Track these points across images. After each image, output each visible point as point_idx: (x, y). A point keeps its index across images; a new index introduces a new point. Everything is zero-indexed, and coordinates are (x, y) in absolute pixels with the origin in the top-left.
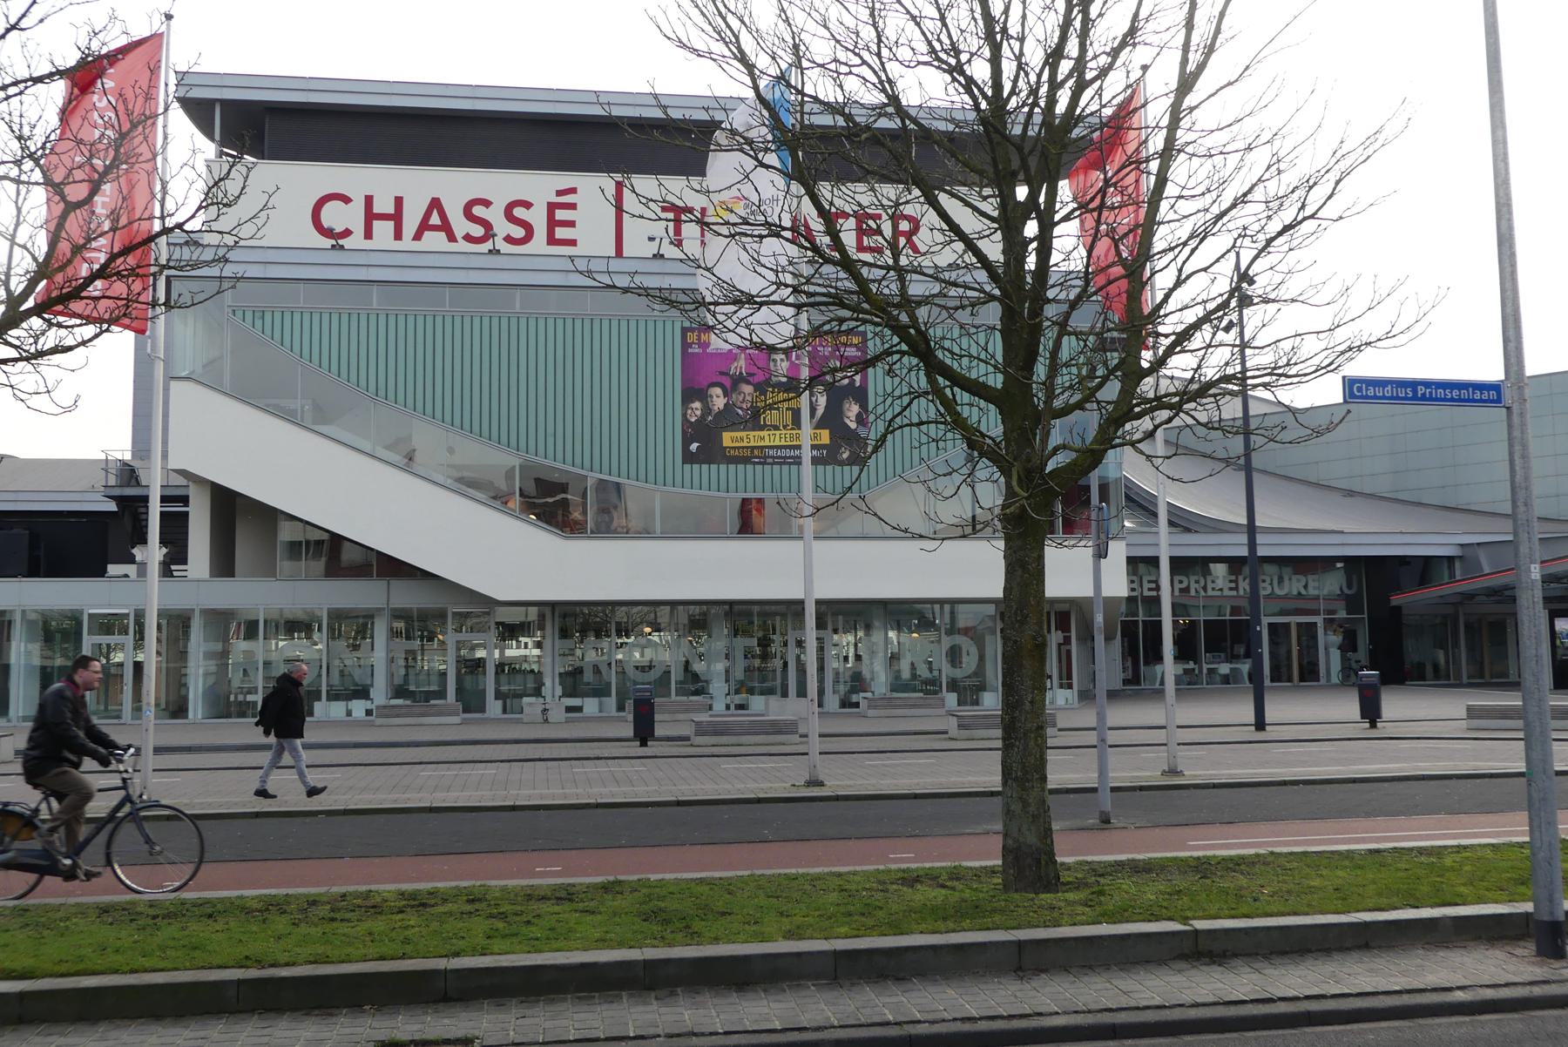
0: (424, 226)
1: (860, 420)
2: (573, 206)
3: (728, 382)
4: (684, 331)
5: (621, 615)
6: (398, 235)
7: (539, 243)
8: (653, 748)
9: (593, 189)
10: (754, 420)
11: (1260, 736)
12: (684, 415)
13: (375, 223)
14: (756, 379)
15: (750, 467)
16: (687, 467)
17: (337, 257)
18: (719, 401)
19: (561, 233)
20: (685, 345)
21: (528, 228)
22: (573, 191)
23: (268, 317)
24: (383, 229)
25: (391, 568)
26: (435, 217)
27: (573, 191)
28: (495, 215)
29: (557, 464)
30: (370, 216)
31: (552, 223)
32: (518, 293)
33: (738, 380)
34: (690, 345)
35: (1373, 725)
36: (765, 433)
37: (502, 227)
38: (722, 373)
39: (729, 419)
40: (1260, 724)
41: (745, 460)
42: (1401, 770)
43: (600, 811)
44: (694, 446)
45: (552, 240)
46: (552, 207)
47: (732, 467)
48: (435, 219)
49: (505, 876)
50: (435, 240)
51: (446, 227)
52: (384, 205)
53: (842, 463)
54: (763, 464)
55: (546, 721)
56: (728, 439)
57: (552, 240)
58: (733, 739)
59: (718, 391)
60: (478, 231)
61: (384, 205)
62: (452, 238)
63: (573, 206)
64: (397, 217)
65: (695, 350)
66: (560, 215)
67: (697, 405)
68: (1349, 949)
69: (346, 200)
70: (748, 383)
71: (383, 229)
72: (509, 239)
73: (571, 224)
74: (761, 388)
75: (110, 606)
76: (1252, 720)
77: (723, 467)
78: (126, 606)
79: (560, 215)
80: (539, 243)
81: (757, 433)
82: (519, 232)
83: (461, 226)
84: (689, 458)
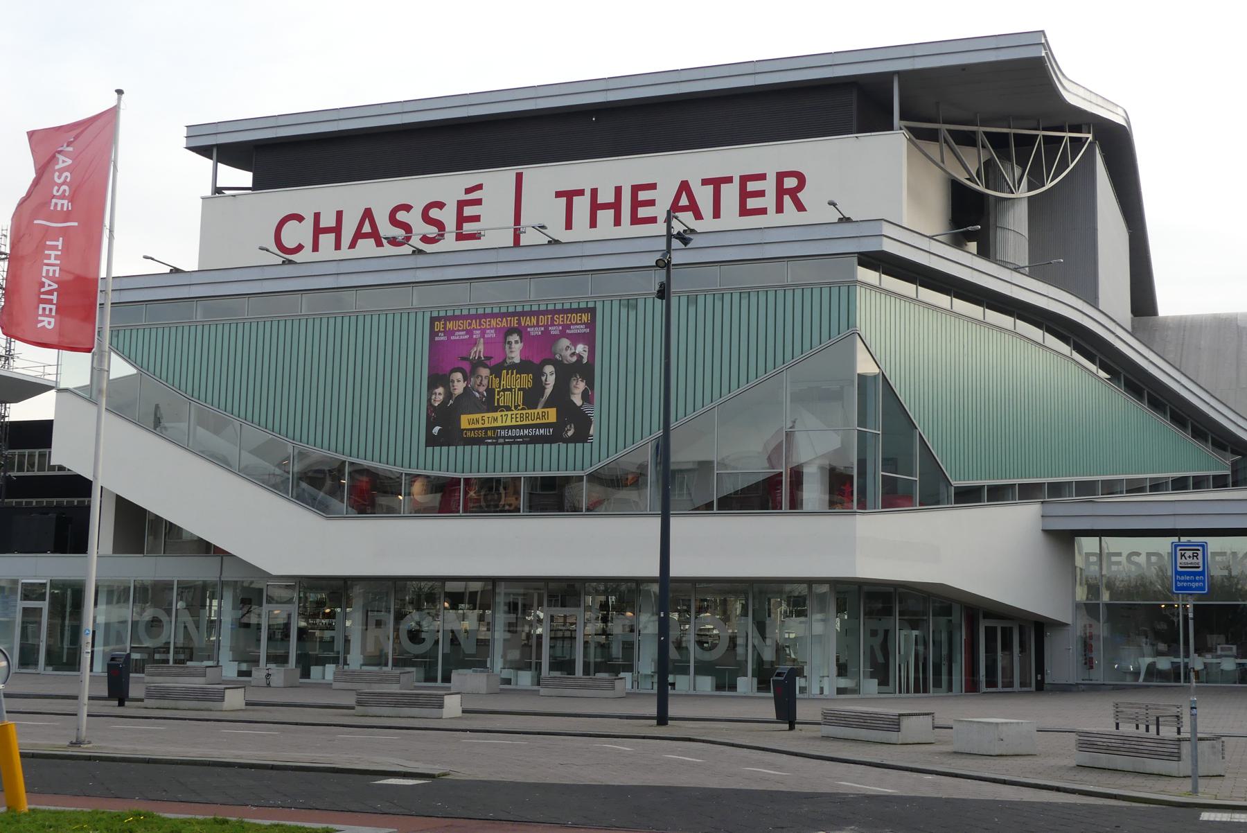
0: (675, 207)
1: (587, 397)
2: (478, 202)
3: (467, 368)
4: (433, 320)
5: (451, 587)
6: (338, 246)
7: (449, 242)
9: (496, 183)
10: (489, 404)
11: (120, 711)
12: (429, 400)
13: (321, 236)
14: (492, 363)
15: (483, 448)
16: (430, 449)
17: (288, 270)
18: (459, 387)
19: (468, 228)
20: (433, 334)
21: (440, 225)
22: (479, 187)
23: (727, 298)
24: (327, 240)
25: (205, 548)
26: (367, 228)
27: (479, 187)
28: (413, 218)
29: (320, 453)
30: (318, 231)
31: (461, 219)
32: (306, 297)
34: (437, 334)
35: (121, 704)
36: (498, 414)
38: (463, 359)
39: (467, 402)
42: (237, 756)
43: (274, 772)
44: (436, 430)
45: (460, 237)
46: (461, 204)
47: (468, 448)
48: (684, 201)
50: (366, 247)
51: (375, 235)
52: (328, 221)
54: (495, 444)
55: (269, 685)
56: (465, 421)
57: (460, 237)
59: (459, 376)
60: (399, 233)
61: (328, 221)
62: (379, 244)
63: (478, 202)
64: (337, 230)
66: (469, 211)
67: (440, 390)
69: (299, 218)
70: (485, 366)
71: (327, 240)
72: (425, 239)
73: (476, 219)
74: (497, 371)
75: (35, 577)
77: (460, 448)
78: (45, 577)
80: (449, 242)
81: (490, 415)
83: (386, 229)
84: (431, 441)
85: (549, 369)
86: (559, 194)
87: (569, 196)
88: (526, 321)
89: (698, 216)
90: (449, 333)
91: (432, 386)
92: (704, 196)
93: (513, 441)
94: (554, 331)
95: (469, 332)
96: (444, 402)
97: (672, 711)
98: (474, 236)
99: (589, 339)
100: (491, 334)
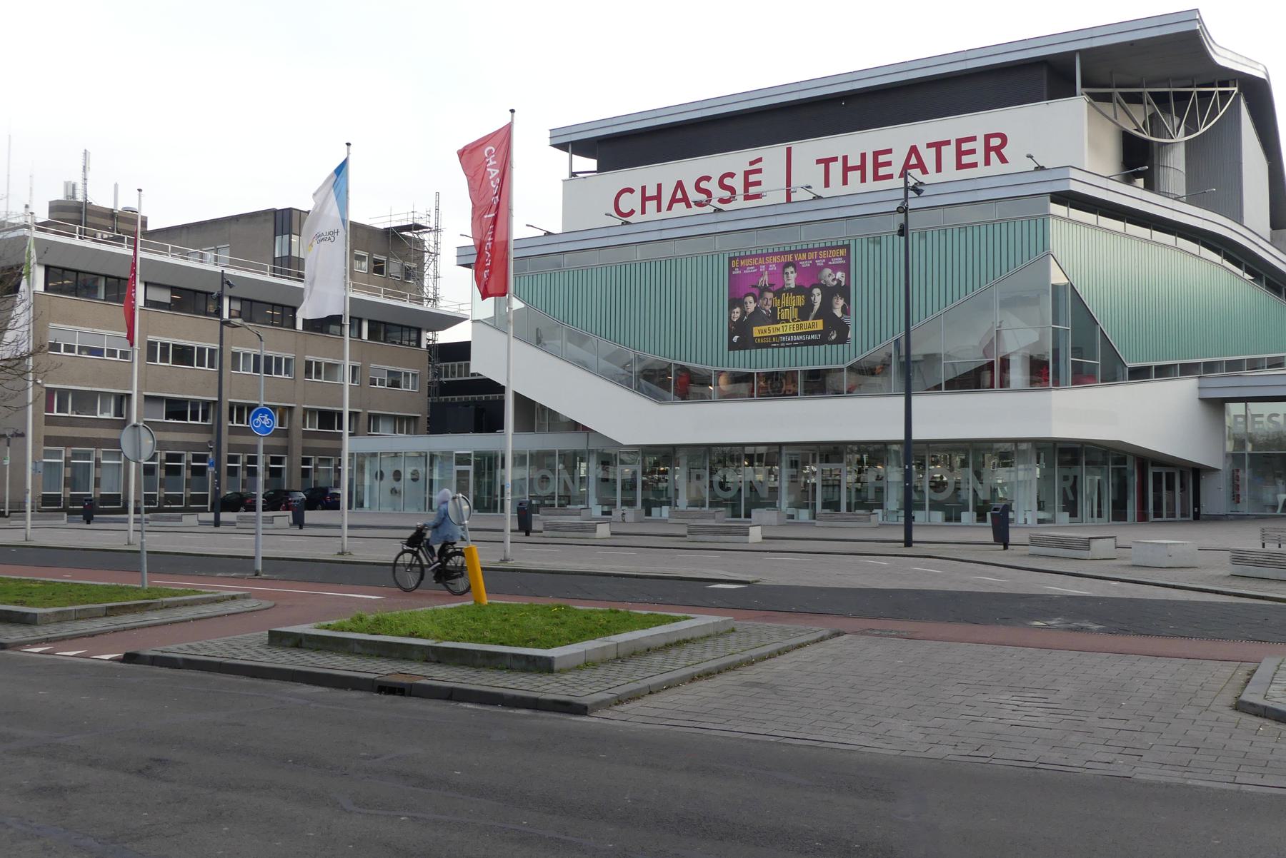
0: (674, 200)
1: (845, 310)
2: (759, 171)
3: (756, 292)
4: (731, 259)
8: (533, 537)
9: (772, 155)
10: (774, 318)
11: (908, 551)
14: (775, 288)
15: (770, 350)
17: (626, 229)
18: (751, 307)
20: (731, 269)
21: (732, 190)
22: (760, 160)
23: (949, 232)
25: (575, 426)
27: (760, 160)
28: (713, 186)
29: (654, 357)
30: (645, 199)
31: (747, 185)
33: (765, 289)
35: (527, 534)
37: (718, 193)
39: (757, 318)
40: (908, 542)
41: (767, 346)
46: (747, 173)
48: (679, 195)
49: (67, 577)
50: (680, 208)
51: (685, 199)
53: (831, 343)
56: (756, 332)
58: (561, 534)
59: (751, 299)
61: (652, 191)
62: (689, 206)
63: (759, 171)
64: (658, 198)
65: (737, 272)
66: (752, 178)
67: (738, 309)
68: (502, 669)
69: (631, 191)
70: (770, 291)
71: (651, 205)
73: (759, 183)
74: (778, 294)
76: (902, 537)
79: (752, 178)
80: (740, 203)
82: (727, 194)
83: (694, 195)
84: (732, 346)
85: (817, 291)
86: (819, 162)
87: (826, 162)
88: (798, 257)
89: (925, 172)
90: (742, 268)
91: (731, 307)
92: (929, 156)
93: (792, 344)
94: (820, 263)
95: (757, 267)
96: (740, 319)
97: (915, 537)
98: (758, 196)
99: (846, 268)
100: (773, 267)
